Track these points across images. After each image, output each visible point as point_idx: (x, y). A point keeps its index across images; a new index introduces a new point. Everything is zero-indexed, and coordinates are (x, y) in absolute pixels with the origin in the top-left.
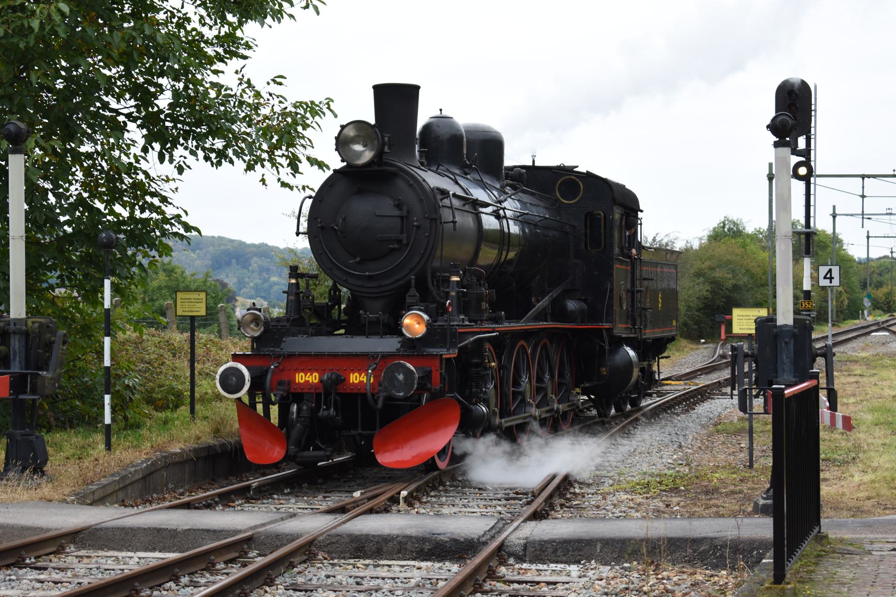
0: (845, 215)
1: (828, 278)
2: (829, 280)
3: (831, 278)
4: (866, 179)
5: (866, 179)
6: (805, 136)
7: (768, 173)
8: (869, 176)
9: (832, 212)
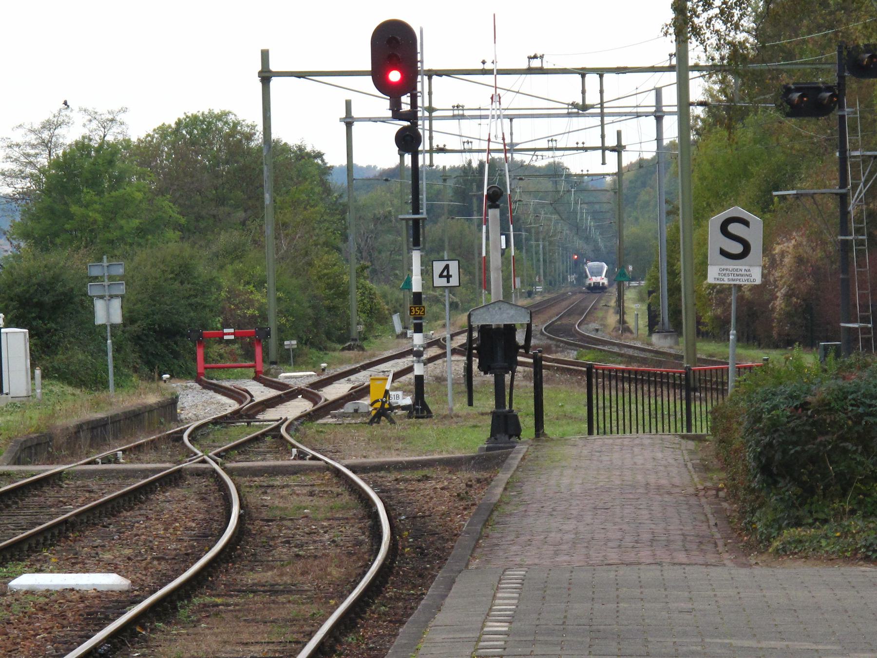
0: (370, 119)
1: (444, 277)
2: (446, 279)
3: (448, 277)
4: (435, 78)
5: (435, 78)
6: (409, 94)
7: (260, 68)
8: (440, 73)
9: (344, 115)
